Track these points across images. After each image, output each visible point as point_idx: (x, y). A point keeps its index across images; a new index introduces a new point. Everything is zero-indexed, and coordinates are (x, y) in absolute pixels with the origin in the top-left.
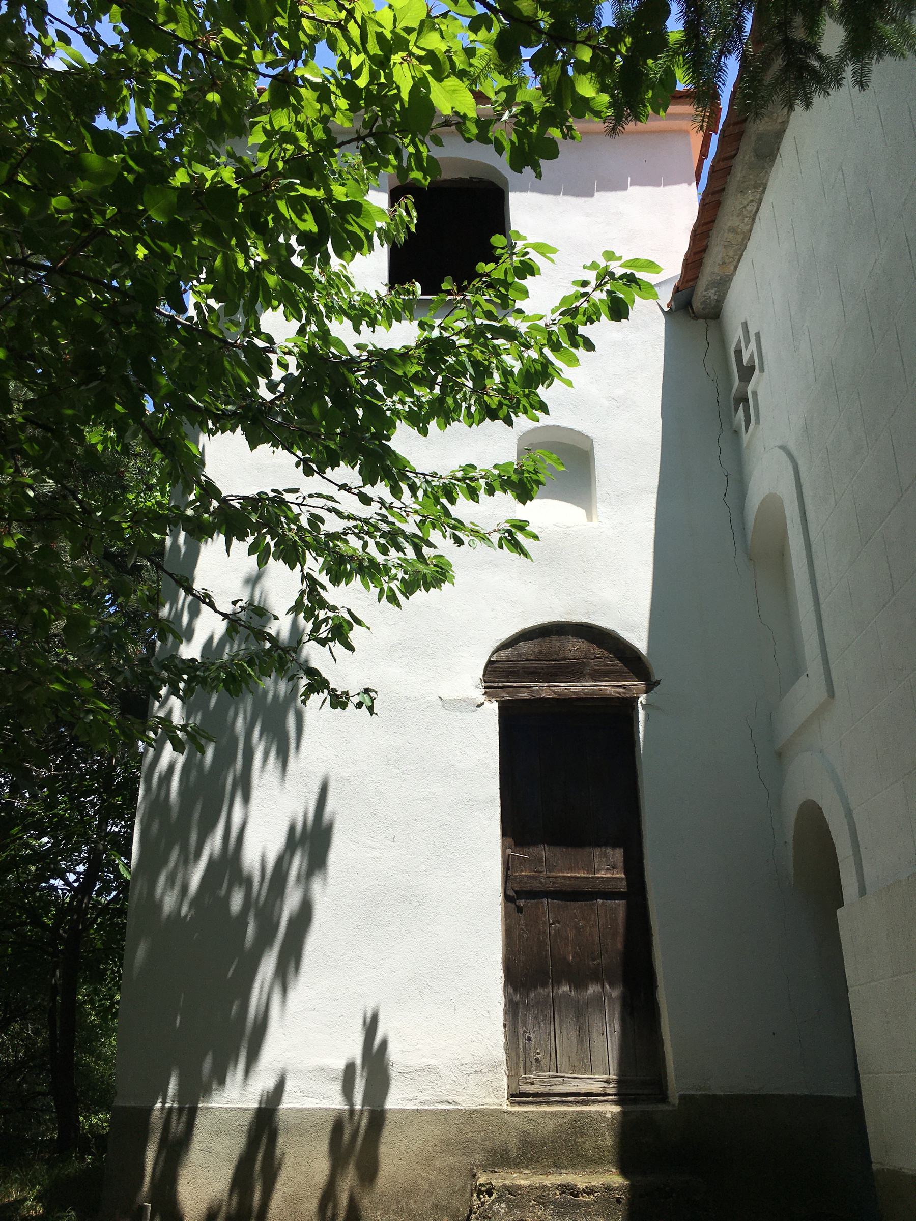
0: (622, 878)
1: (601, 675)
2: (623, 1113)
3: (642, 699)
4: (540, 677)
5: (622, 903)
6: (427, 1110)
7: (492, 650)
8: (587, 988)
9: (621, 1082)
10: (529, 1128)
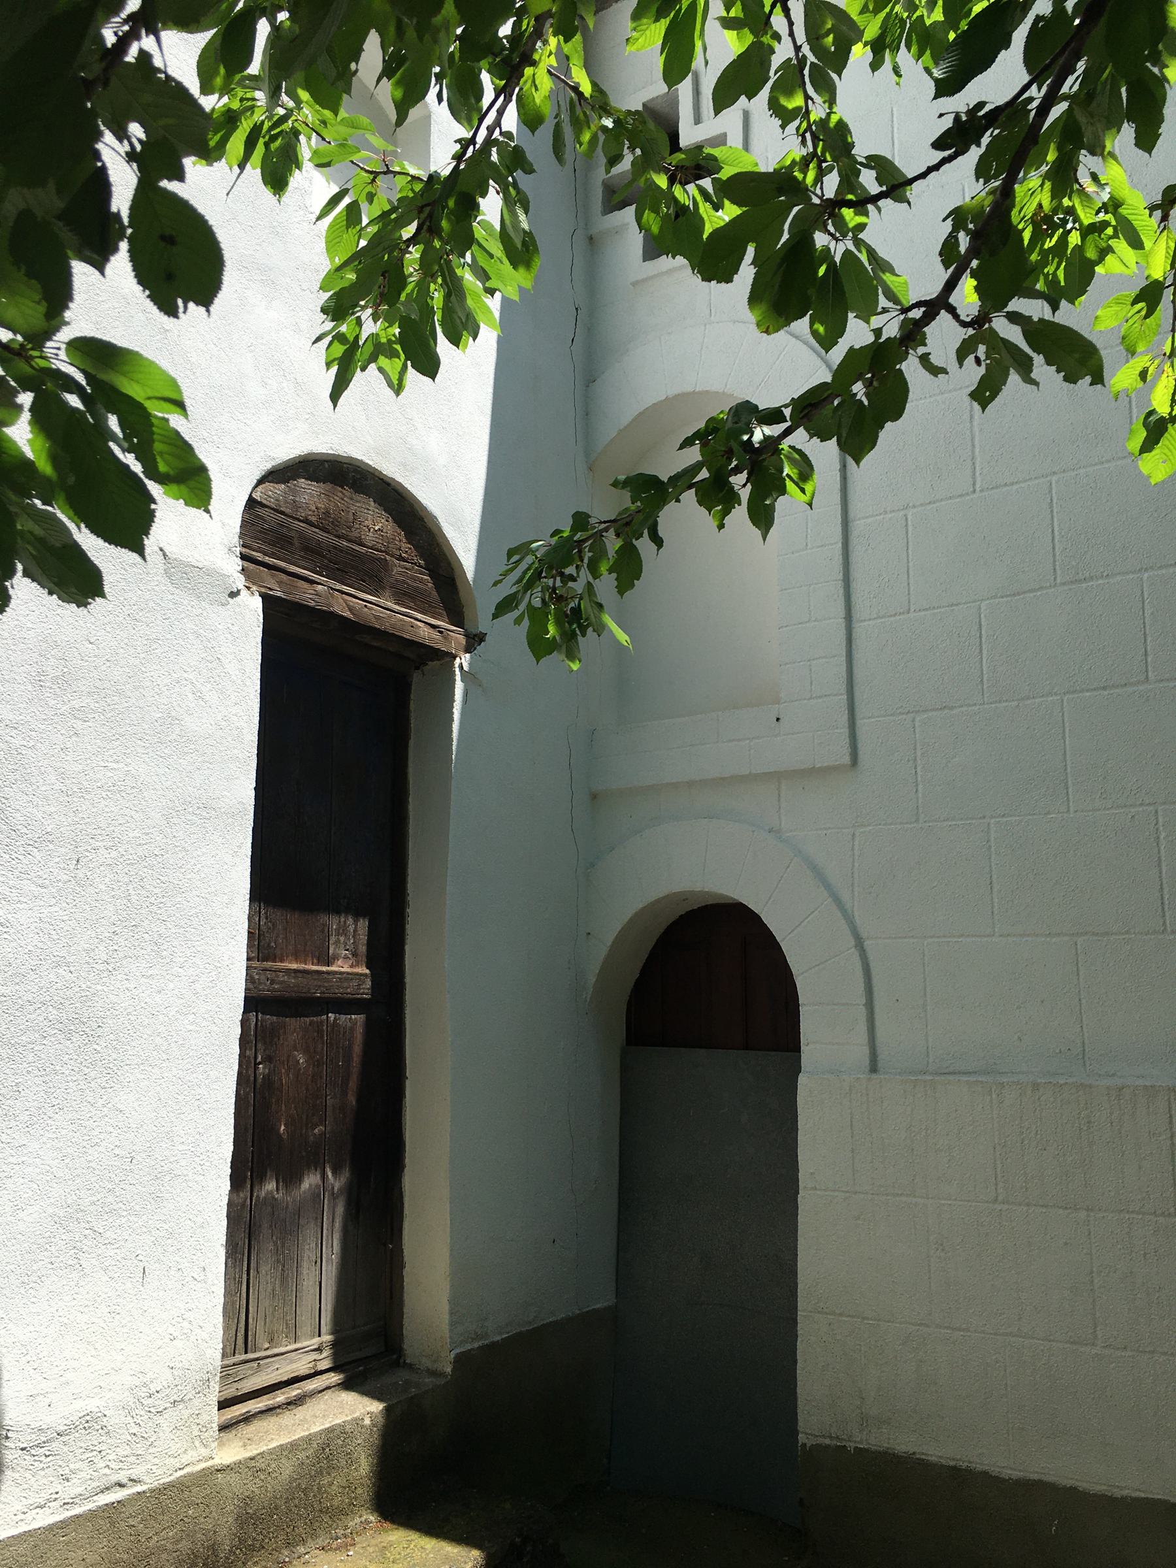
0: (366, 975)
1: (412, 597)
2: (388, 1411)
3: (464, 660)
4: (326, 568)
5: (359, 1018)
6: (78, 1516)
7: (257, 475)
8: (301, 1181)
9: (337, 1346)
10: (253, 1487)
